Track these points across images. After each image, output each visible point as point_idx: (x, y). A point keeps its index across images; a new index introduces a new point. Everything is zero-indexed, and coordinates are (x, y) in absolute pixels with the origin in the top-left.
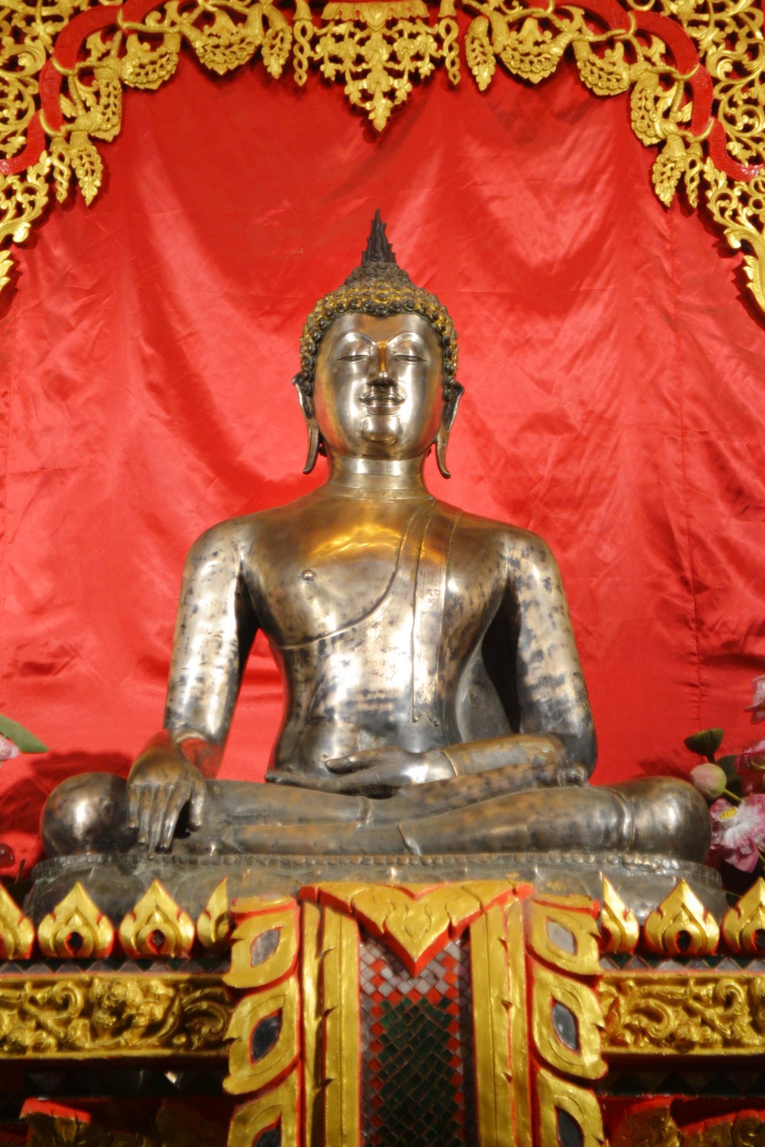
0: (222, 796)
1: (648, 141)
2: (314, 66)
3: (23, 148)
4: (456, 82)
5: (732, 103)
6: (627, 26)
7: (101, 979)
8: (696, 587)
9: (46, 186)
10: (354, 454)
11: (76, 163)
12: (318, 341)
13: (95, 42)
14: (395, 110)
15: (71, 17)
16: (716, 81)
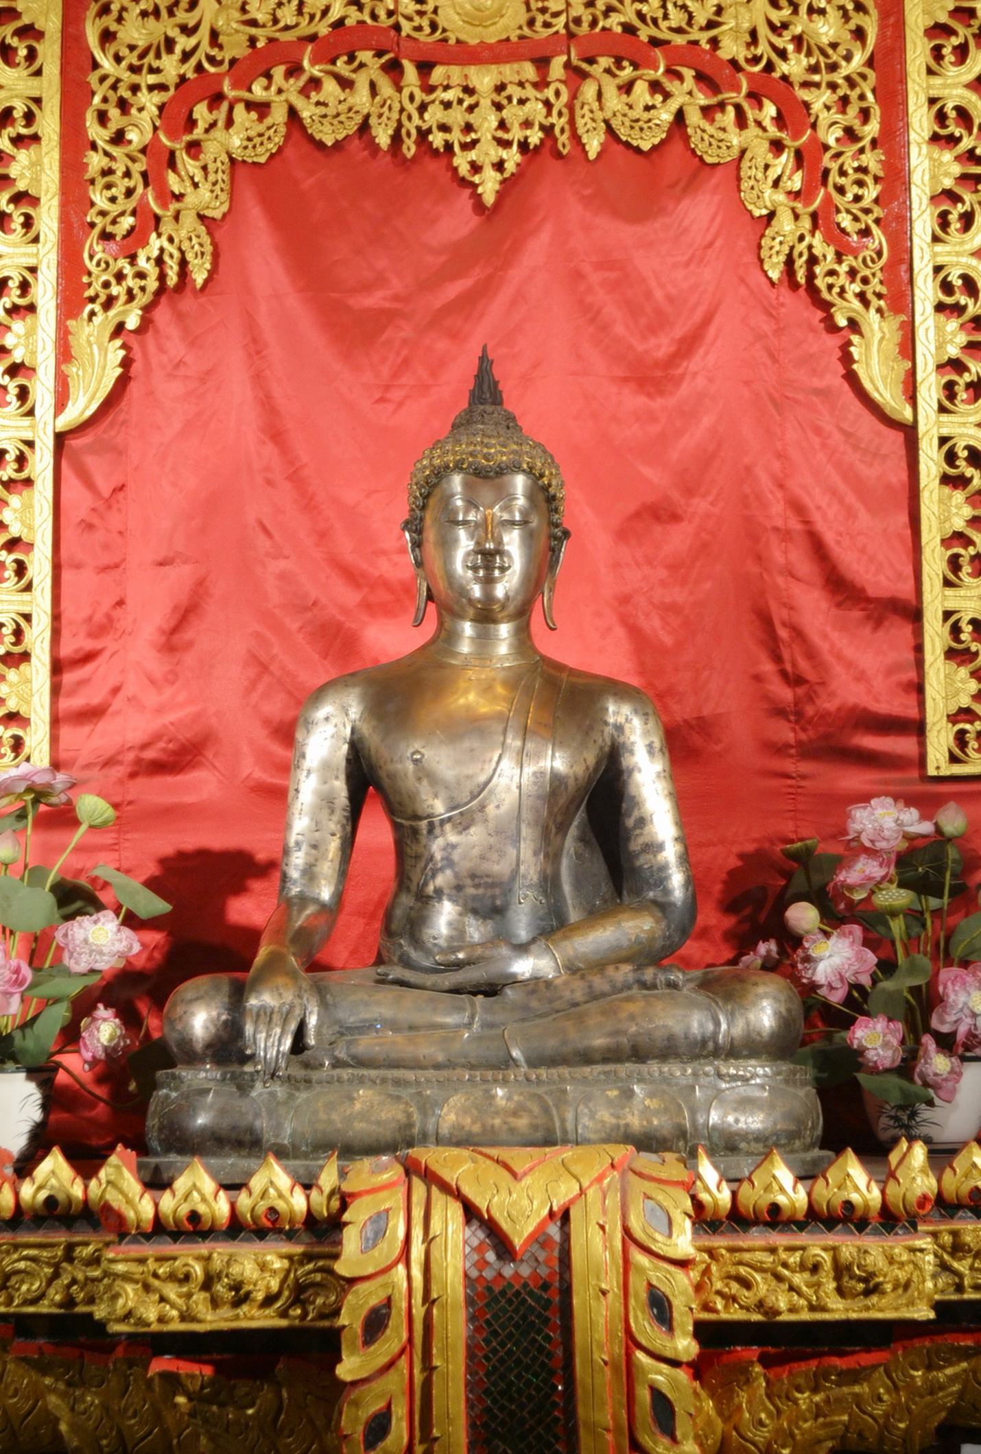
0: (335, 1005)
1: (757, 213)
2: (423, 134)
3: (132, 230)
4: (565, 152)
5: (842, 173)
6: (737, 88)
7: (219, 1254)
8: (795, 680)
9: (157, 270)
10: (462, 617)
11: (185, 246)
12: (426, 497)
13: (201, 112)
14: (504, 182)
15: (177, 86)
16: (826, 148)
